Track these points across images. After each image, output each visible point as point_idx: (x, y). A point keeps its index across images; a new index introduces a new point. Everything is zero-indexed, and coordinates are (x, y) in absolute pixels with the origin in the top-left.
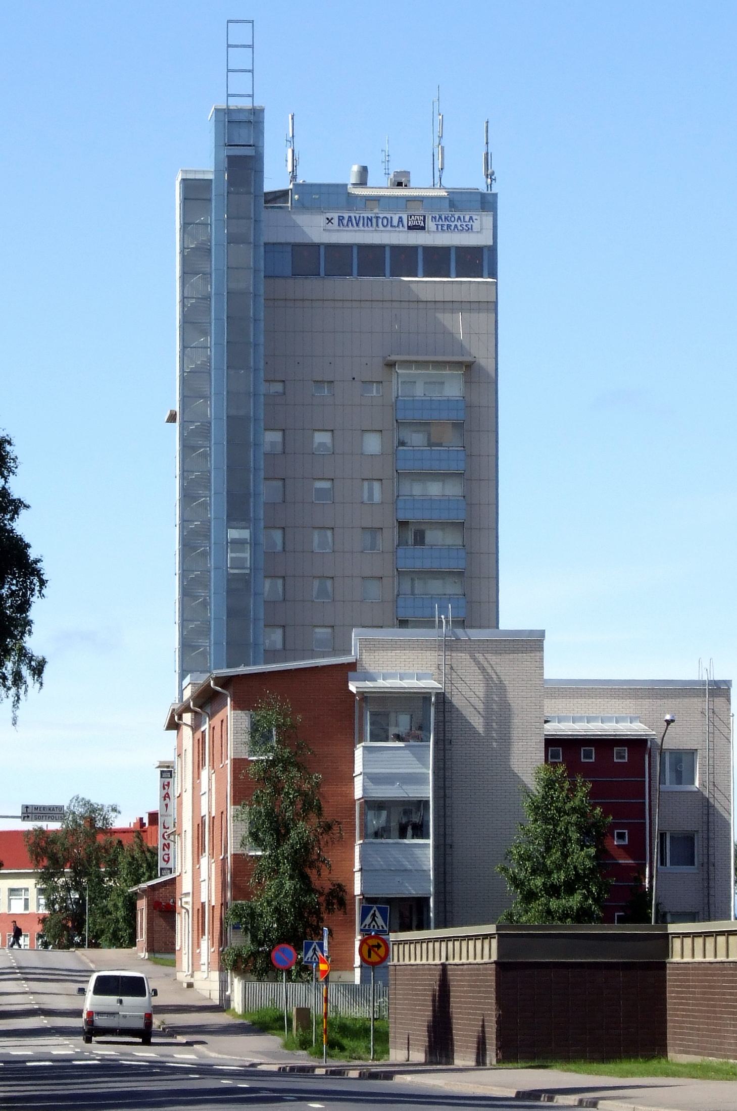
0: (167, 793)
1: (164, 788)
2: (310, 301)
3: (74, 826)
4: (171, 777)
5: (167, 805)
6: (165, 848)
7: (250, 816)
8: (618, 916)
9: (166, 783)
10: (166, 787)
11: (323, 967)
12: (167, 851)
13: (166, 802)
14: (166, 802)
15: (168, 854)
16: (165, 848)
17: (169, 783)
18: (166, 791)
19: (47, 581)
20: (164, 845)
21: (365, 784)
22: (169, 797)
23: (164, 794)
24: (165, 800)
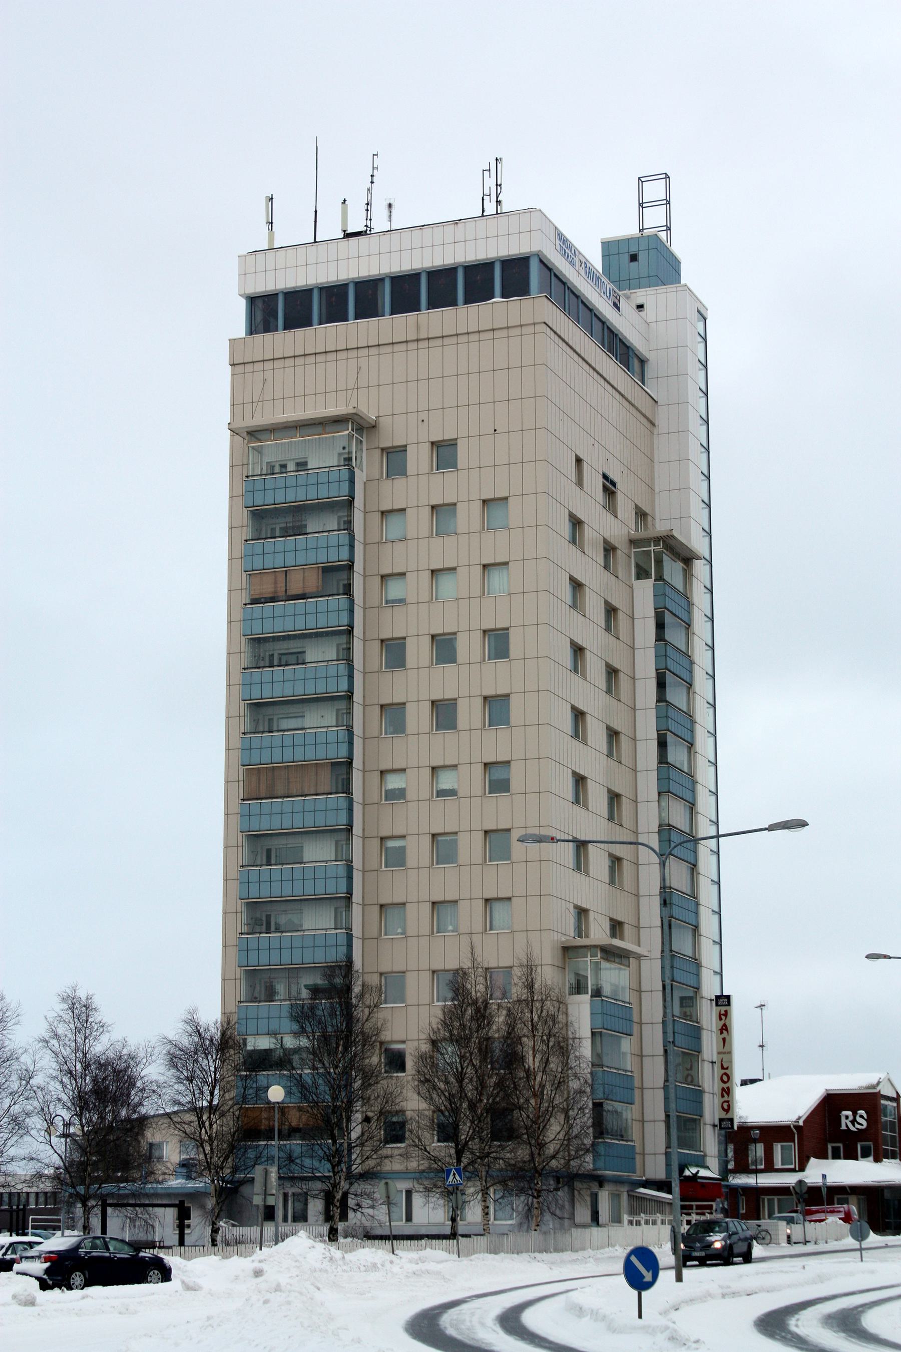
0: (725, 1025)
1: (721, 1019)
2: (427, 341)
3: (518, 1076)
4: (729, 1004)
5: (724, 1039)
6: (724, 1093)
7: (309, 1038)
8: (839, 1147)
9: (723, 1012)
10: (723, 1017)
11: (123, 1113)
12: (726, 1098)
13: (723, 1036)
14: (723, 1036)
15: (728, 1102)
16: (724, 1093)
17: (726, 1011)
18: (722, 1022)
19: (64, 1000)
20: (723, 1089)
21: (692, 907)
22: (727, 1030)
23: (721, 1025)
24: (722, 1033)
